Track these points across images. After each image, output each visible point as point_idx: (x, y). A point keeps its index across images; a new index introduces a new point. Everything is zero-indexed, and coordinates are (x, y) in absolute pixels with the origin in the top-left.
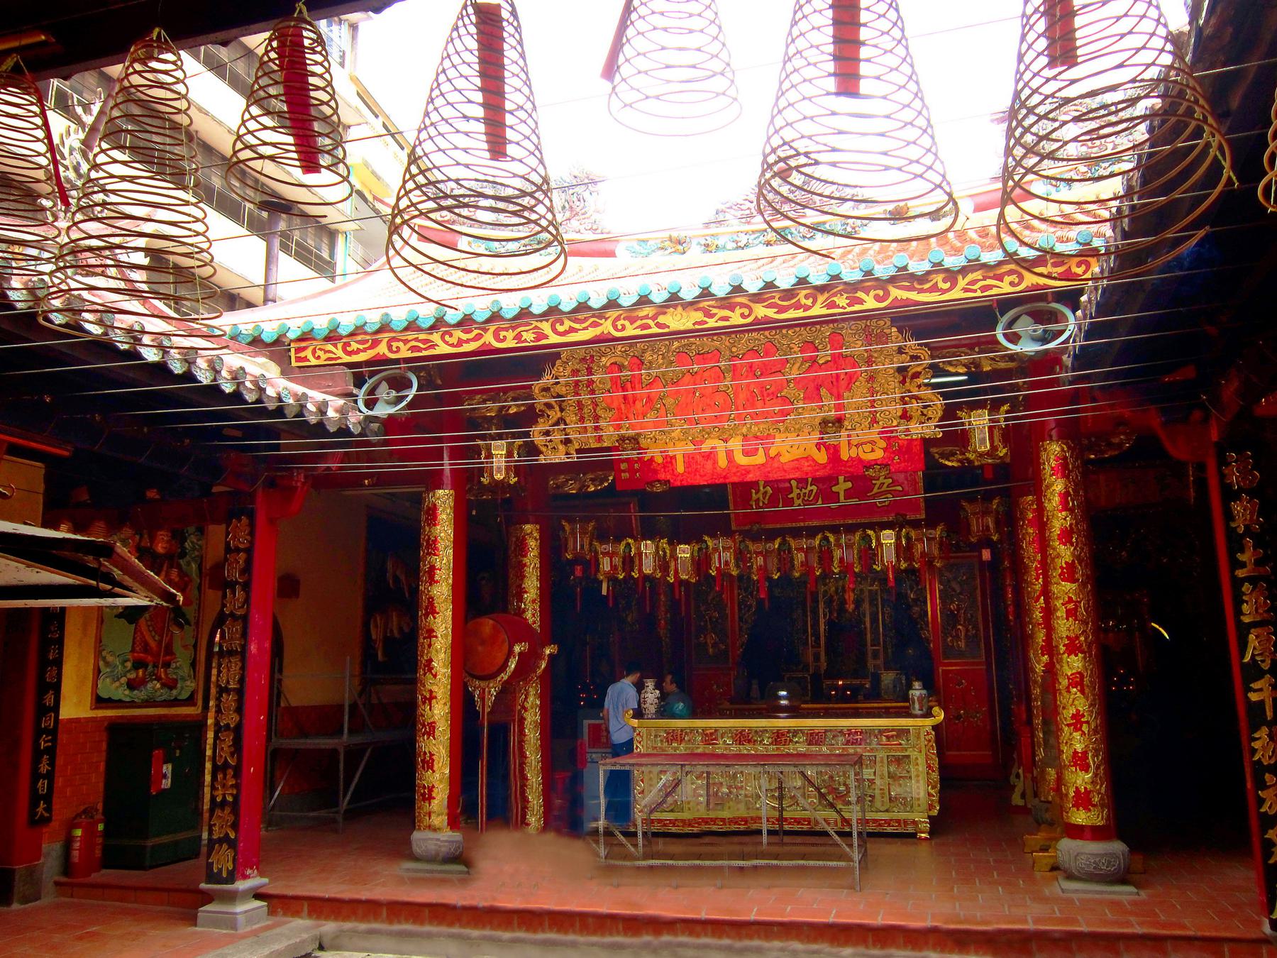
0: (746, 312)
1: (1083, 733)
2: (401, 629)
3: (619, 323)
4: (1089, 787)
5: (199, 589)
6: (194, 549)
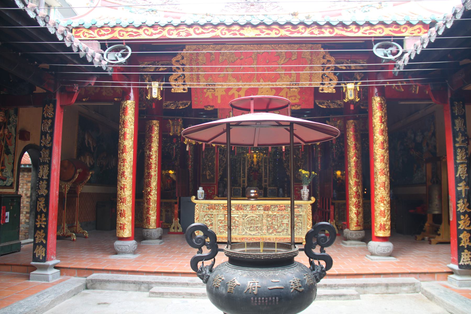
0: (278, 32)
1: (384, 204)
2: (90, 164)
3: (223, 32)
4: (385, 223)
5: (15, 138)
6: (13, 121)
